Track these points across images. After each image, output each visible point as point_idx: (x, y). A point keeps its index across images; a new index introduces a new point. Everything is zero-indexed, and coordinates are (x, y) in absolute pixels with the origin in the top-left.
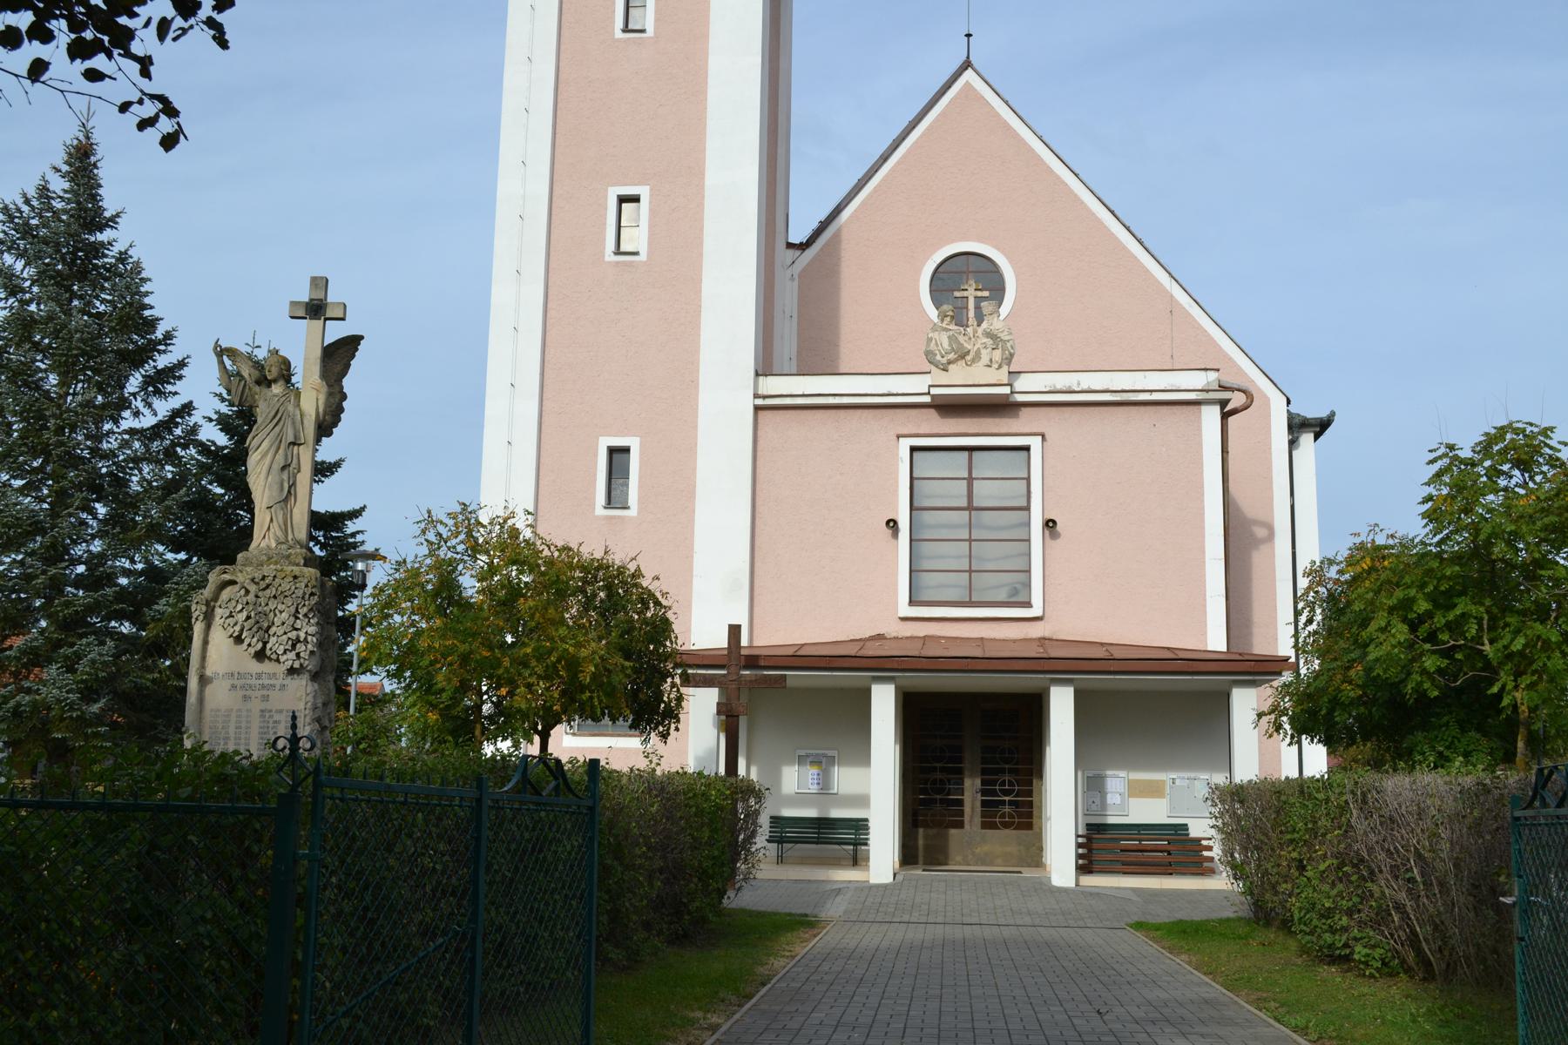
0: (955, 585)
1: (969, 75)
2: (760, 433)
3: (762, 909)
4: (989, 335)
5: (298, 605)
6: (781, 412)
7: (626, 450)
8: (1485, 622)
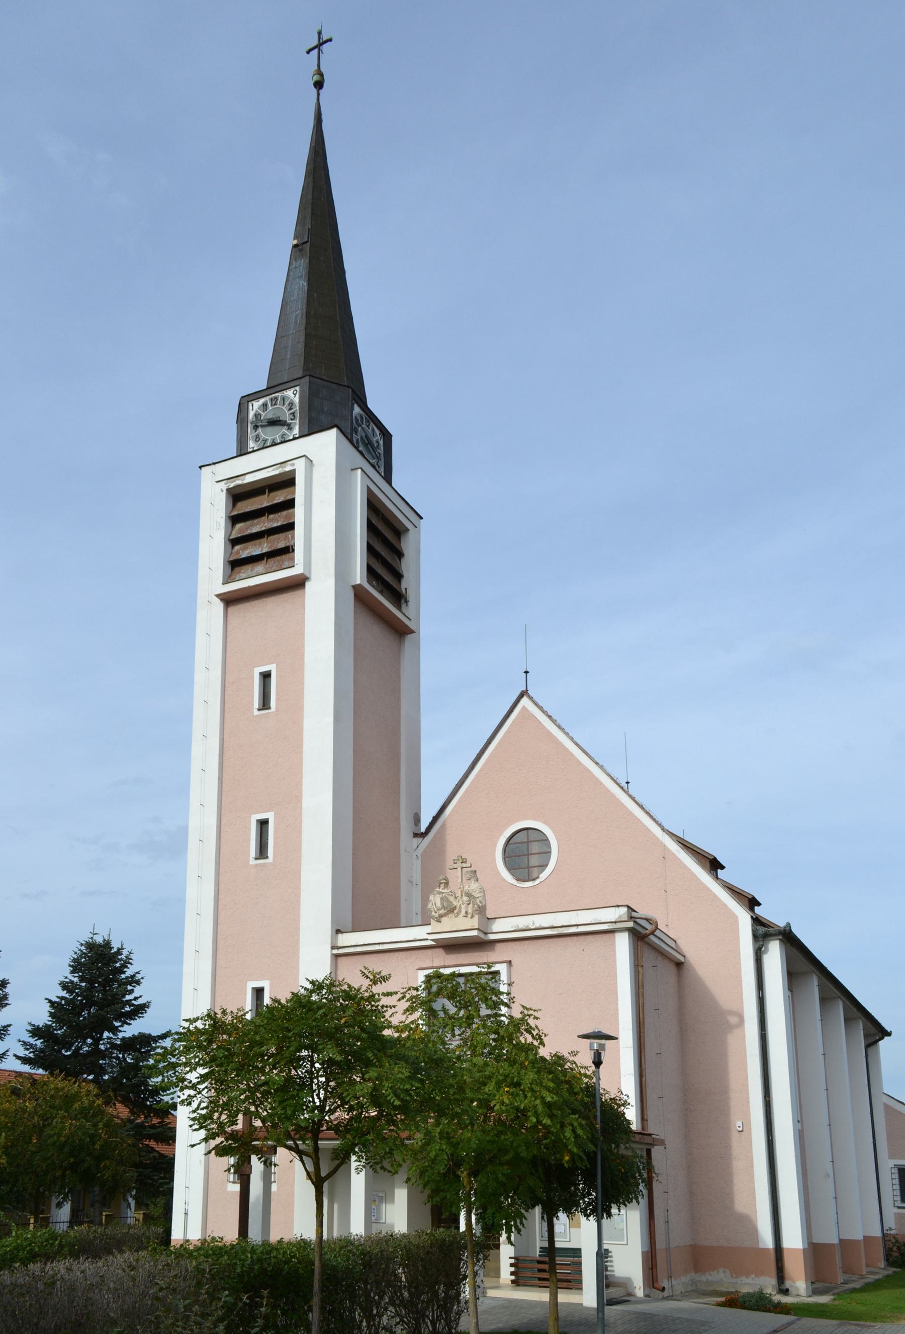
1: (525, 701)
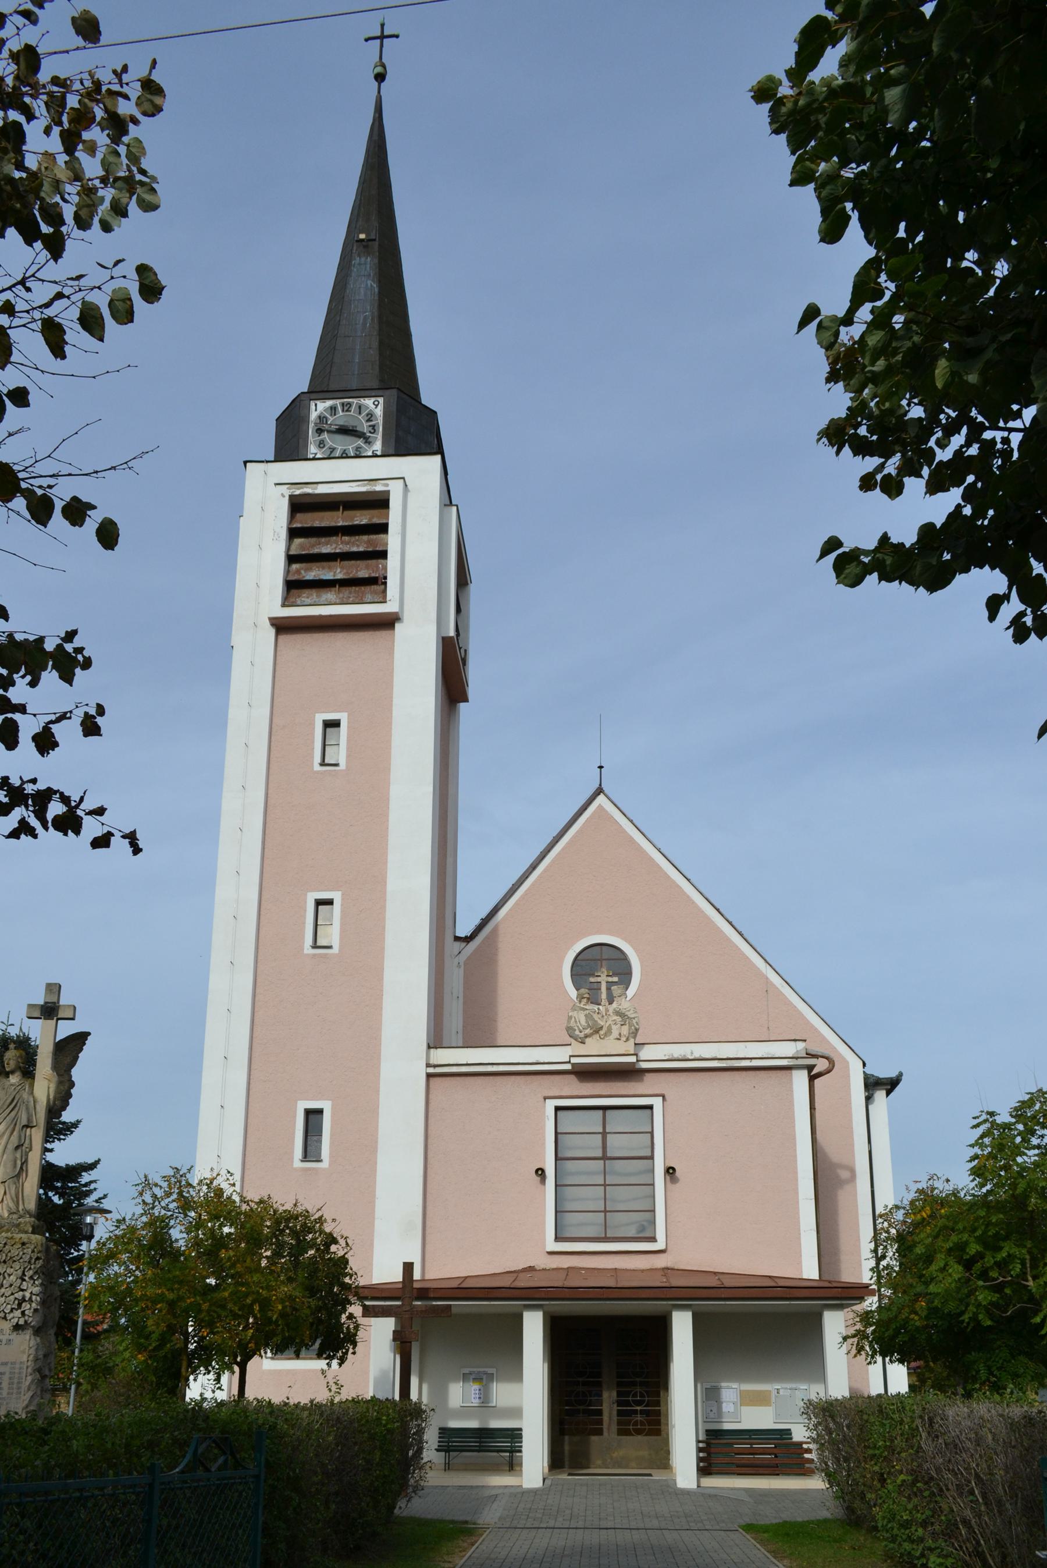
0: (593, 1224)
1: (601, 799)
2: (431, 1096)
3: (429, 1517)
4: (618, 1013)
5: (25, 1268)
6: (448, 1078)
7: (320, 1112)
8: (1028, 1261)
